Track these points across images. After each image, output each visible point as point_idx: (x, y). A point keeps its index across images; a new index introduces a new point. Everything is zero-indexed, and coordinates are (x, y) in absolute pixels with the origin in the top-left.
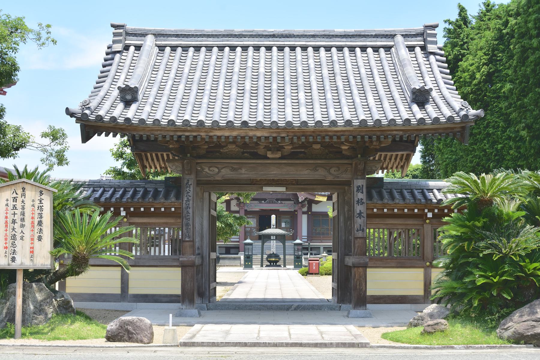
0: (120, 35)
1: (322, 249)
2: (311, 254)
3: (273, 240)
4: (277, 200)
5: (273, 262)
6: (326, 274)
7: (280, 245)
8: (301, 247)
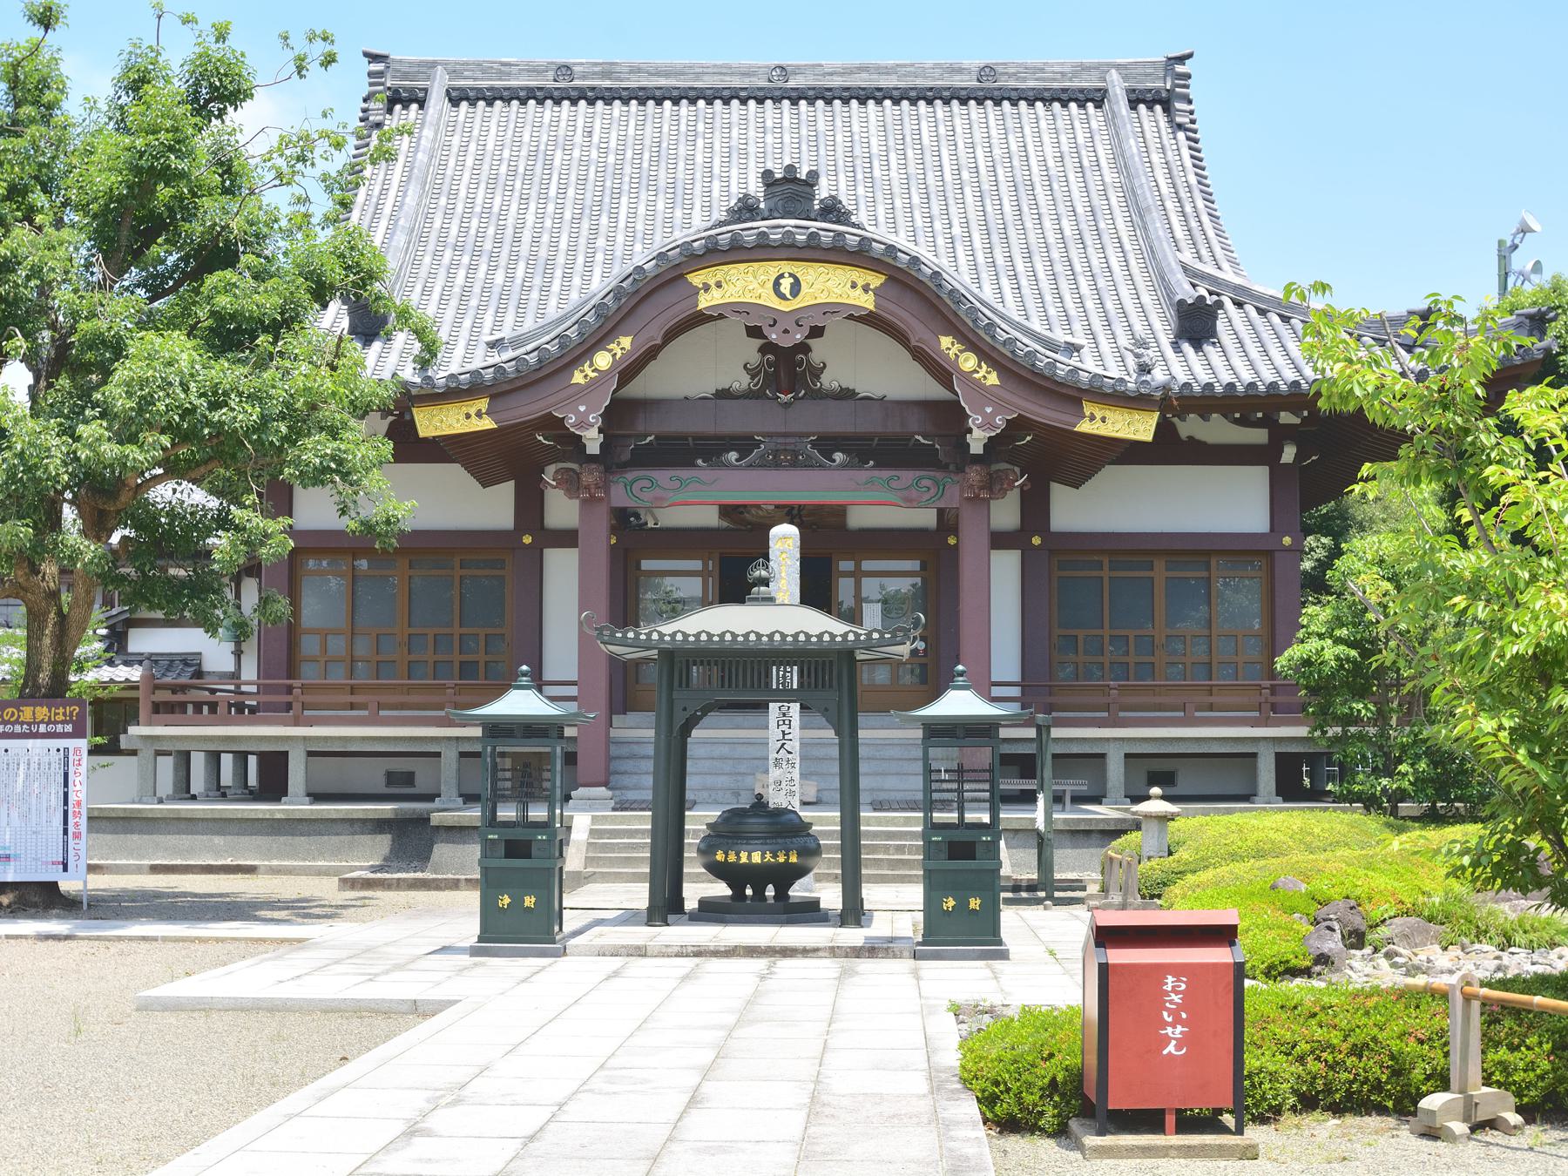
0: (380, 74)
1: (1115, 770)
2: (1058, 799)
3: (786, 695)
4: (827, 444)
5: (758, 876)
6: (1308, 1102)
7: (821, 743)
8: (982, 756)
